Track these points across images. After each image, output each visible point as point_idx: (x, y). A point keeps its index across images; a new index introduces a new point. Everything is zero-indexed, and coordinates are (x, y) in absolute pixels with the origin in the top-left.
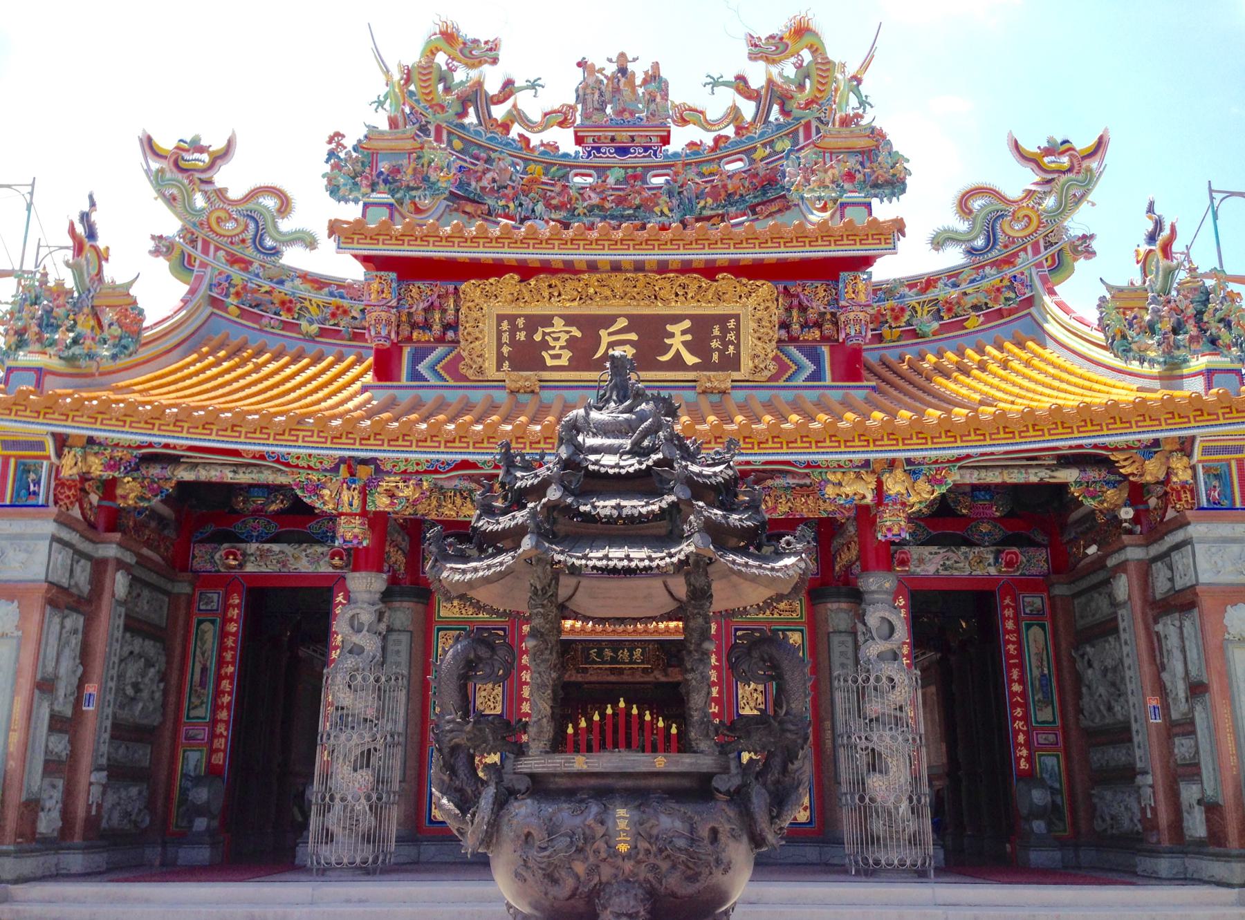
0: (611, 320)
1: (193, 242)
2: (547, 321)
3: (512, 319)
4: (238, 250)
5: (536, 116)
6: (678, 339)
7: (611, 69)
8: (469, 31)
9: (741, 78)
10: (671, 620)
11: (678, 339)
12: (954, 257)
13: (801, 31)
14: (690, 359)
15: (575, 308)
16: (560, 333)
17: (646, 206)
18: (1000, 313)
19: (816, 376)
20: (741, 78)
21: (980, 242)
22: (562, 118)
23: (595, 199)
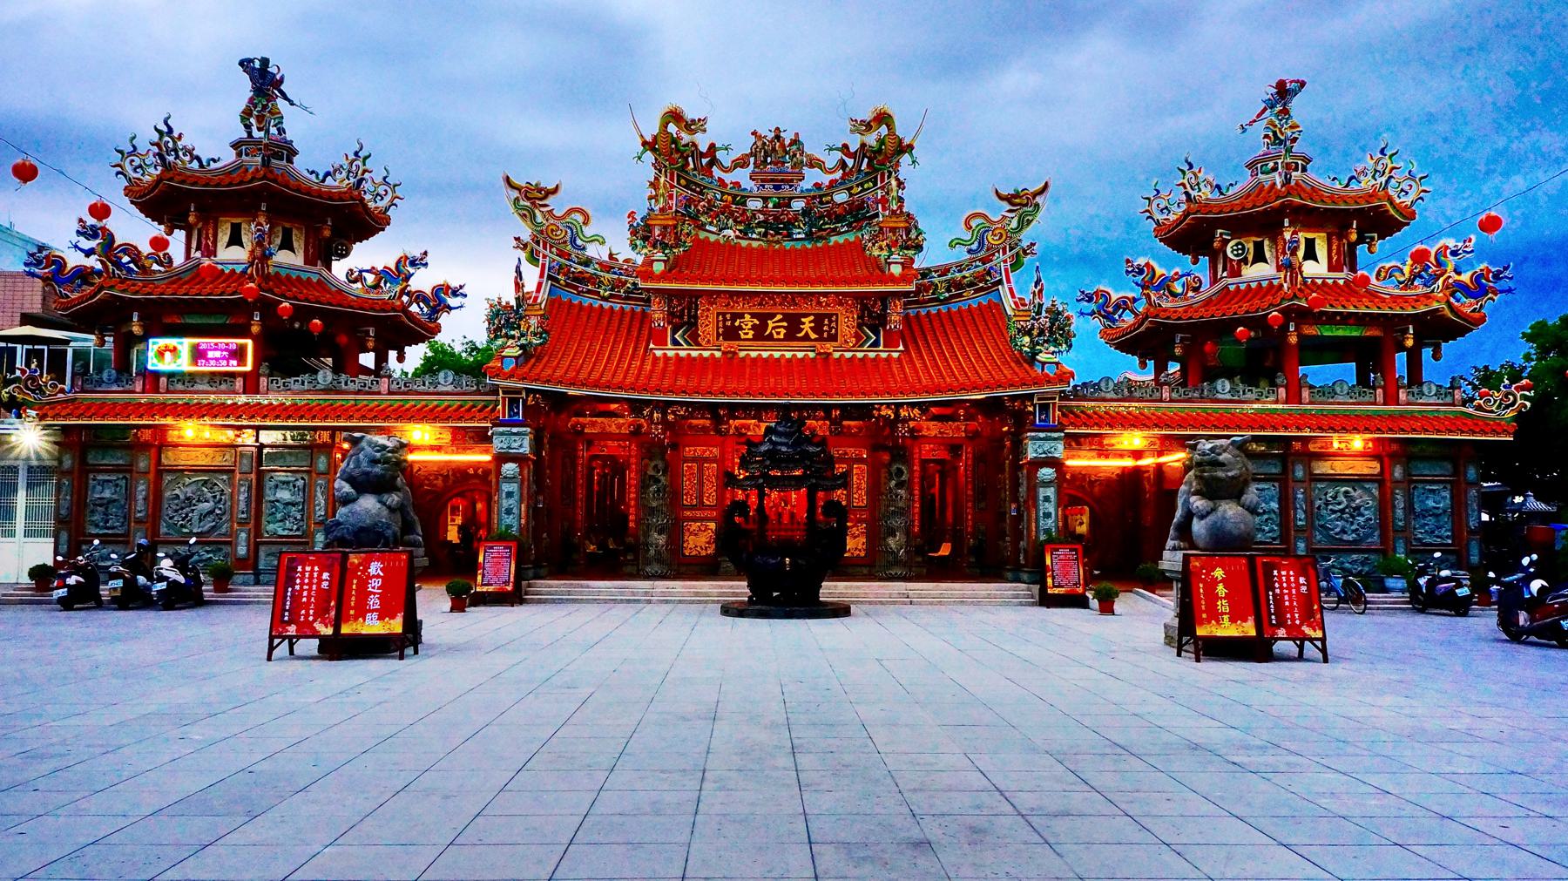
0: (774, 315)
1: (538, 243)
2: (741, 316)
3: (724, 315)
4: (561, 247)
5: (727, 164)
6: (807, 324)
7: (771, 135)
8: (689, 115)
9: (845, 146)
10: (730, 249)
11: (807, 324)
12: (961, 254)
13: (883, 118)
14: (813, 336)
15: (756, 310)
16: (748, 322)
17: (790, 224)
18: (982, 289)
19: (876, 344)
20: (845, 146)
21: (974, 247)
22: (741, 163)
23: (762, 217)
